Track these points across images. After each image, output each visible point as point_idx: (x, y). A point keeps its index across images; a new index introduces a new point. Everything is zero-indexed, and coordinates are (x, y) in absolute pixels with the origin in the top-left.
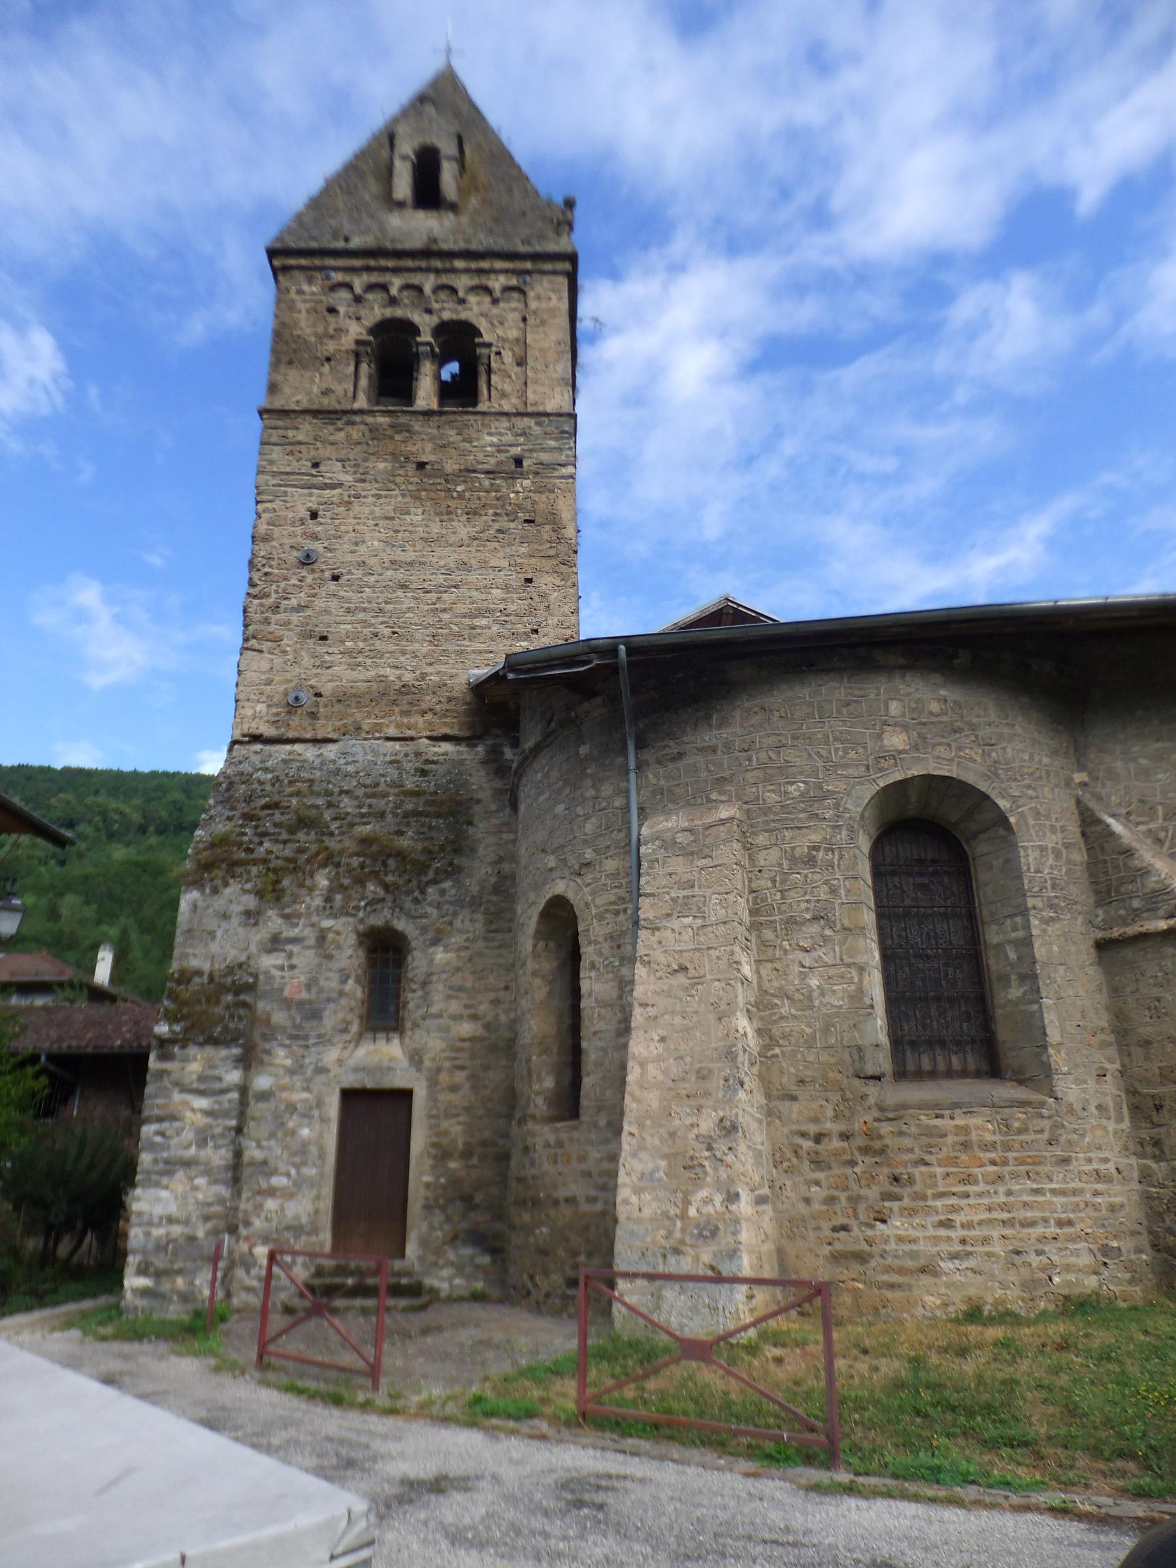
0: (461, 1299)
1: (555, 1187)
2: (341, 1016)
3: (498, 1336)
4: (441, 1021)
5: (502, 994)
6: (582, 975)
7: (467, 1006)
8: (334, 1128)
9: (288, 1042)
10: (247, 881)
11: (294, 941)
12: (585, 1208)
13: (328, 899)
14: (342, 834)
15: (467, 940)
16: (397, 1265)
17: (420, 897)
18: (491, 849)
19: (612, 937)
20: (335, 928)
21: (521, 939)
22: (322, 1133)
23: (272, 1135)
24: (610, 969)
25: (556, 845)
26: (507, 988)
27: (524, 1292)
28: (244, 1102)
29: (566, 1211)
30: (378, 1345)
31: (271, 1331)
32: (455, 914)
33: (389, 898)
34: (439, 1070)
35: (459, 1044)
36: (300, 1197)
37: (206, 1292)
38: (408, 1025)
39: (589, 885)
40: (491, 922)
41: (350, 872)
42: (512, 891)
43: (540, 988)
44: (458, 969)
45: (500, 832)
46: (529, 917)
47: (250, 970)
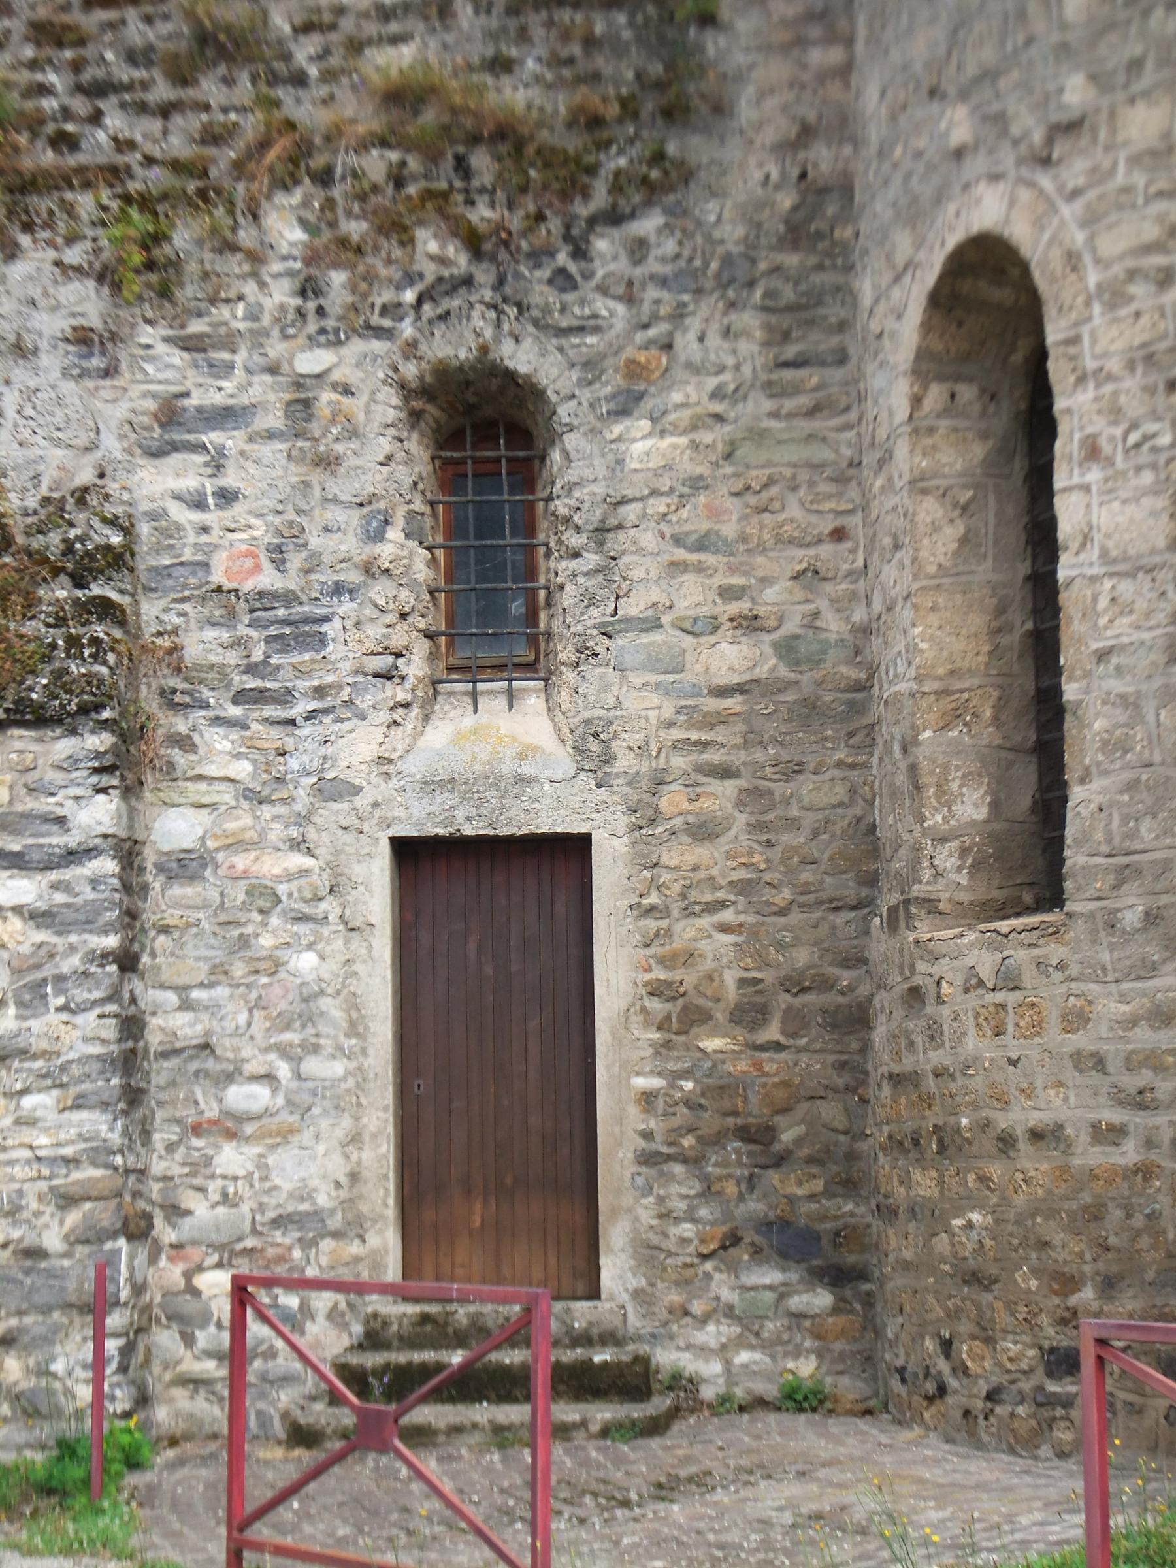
0: (760, 1403)
1: (1002, 1100)
2: (374, 632)
3: (864, 1504)
4: (657, 637)
5: (826, 550)
6: (1059, 481)
7: (727, 593)
8: (382, 946)
9: (235, 711)
10: (71, 240)
11: (225, 416)
12: (1089, 1156)
13: (309, 288)
14: (329, 76)
15: (717, 394)
16: (582, 1313)
17: (573, 268)
18: (772, 103)
19: (1149, 359)
20: (336, 376)
21: (877, 381)
22: (352, 963)
23: (219, 973)
24: (1144, 456)
25: (971, 70)
26: (839, 534)
27: (930, 1387)
28: (131, 883)
29: (1034, 1164)
30: (538, 1527)
31: (256, 1494)
32: (679, 315)
33: (484, 275)
34: (659, 781)
35: (712, 704)
36: (307, 1137)
37: (85, 1393)
38: (566, 653)
39: (1075, 194)
40: (786, 337)
41: (362, 197)
42: (844, 233)
43: (936, 528)
44: (697, 484)
45: (800, 42)
46: (895, 308)
47: (109, 510)
